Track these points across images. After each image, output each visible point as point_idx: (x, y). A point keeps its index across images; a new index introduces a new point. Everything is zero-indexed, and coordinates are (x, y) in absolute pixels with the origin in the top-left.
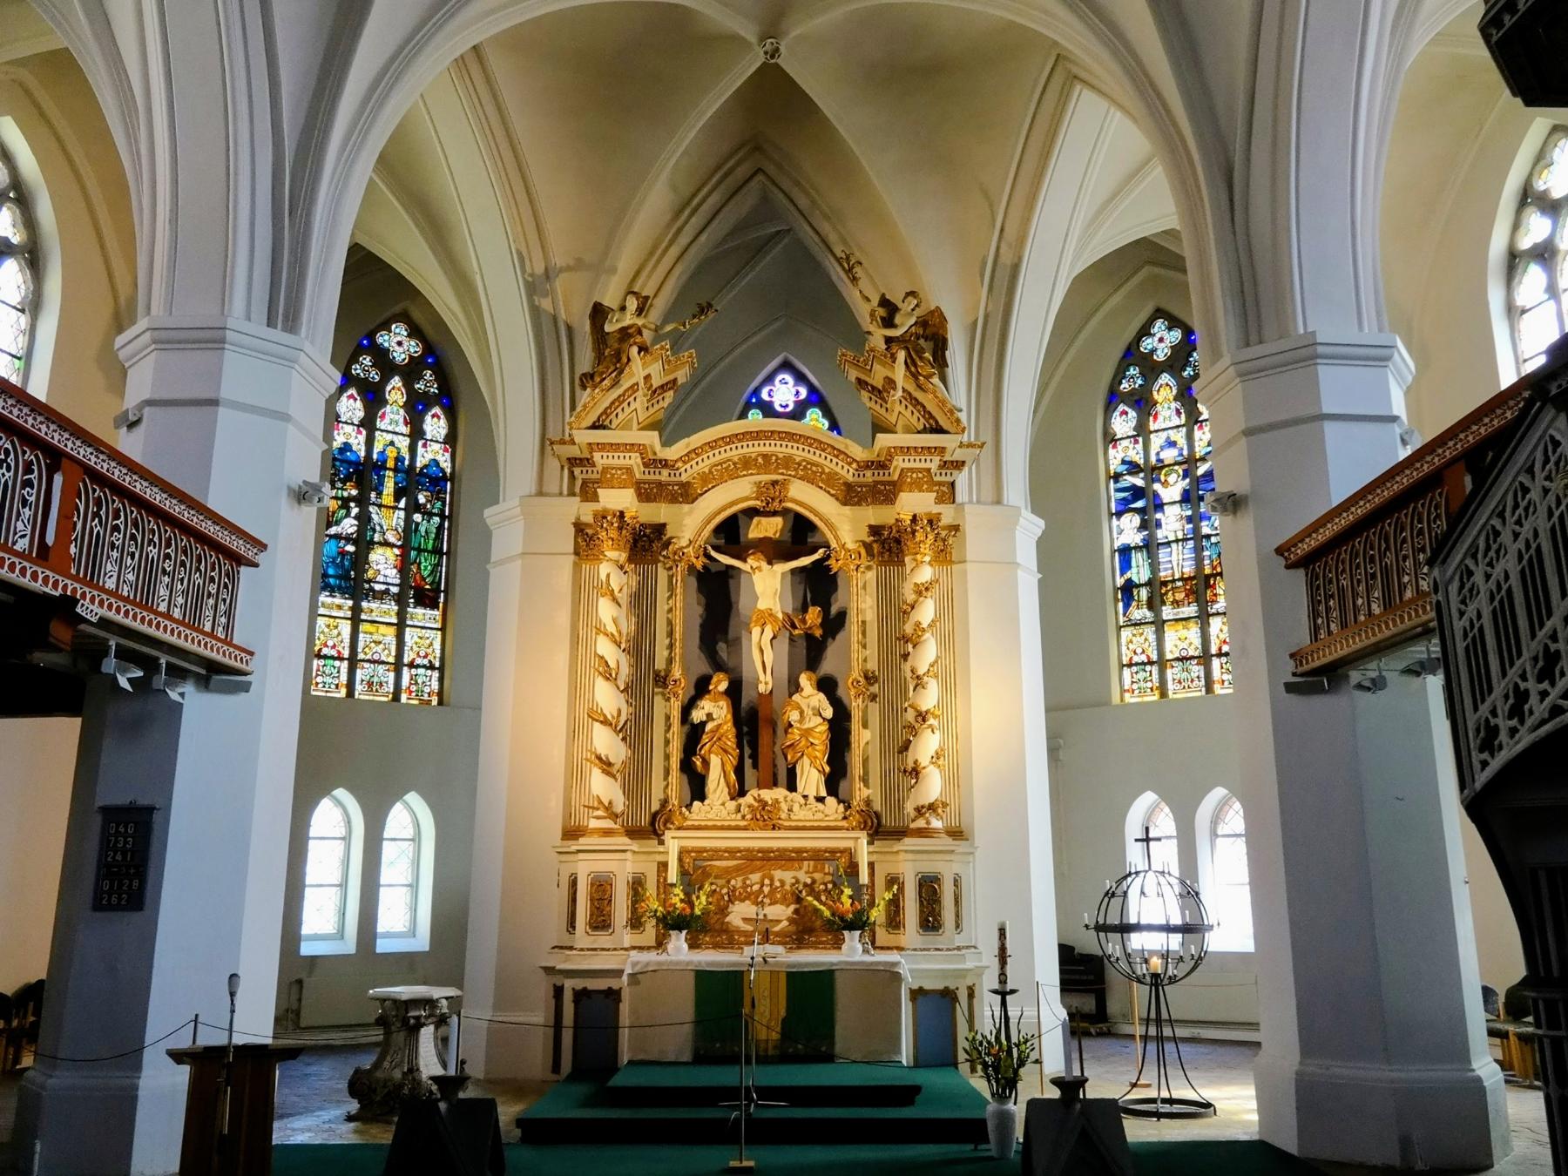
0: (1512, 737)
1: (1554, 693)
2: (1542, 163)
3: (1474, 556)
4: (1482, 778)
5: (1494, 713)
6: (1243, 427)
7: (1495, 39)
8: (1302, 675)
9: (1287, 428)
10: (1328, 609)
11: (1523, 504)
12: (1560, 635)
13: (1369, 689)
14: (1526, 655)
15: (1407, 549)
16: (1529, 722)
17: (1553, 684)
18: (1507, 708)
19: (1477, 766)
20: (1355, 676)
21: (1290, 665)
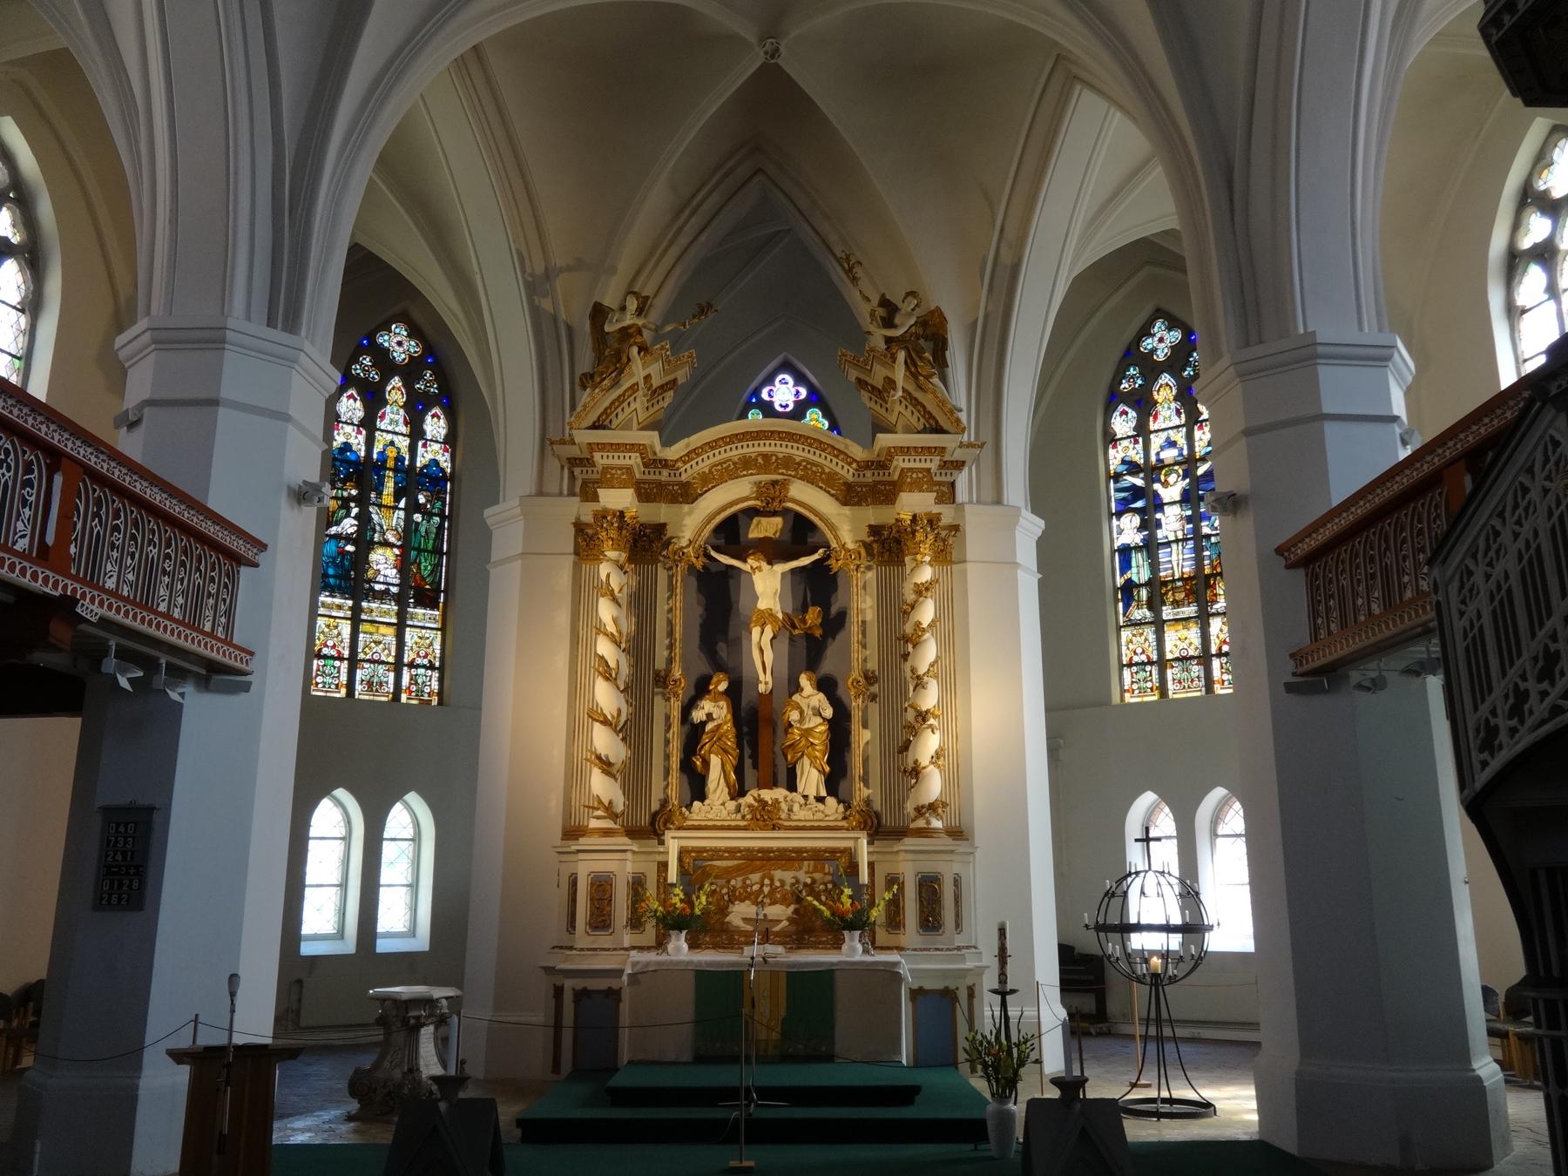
0: (1512, 737)
2: (1543, 163)
3: (1474, 556)
4: (1482, 778)
5: (1494, 713)
6: (1241, 426)
7: (1495, 38)
8: (1302, 675)
9: (1283, 426)
11: (1523, 504)
13: (1369, 689)
14: (1525, 655)
15: (1407, 549)
16: (1529, 722)
17: (1553, 684)
18: (1507, 707)
19: (1477, 766)
20: (1355, 676)
21: (1290, 666)
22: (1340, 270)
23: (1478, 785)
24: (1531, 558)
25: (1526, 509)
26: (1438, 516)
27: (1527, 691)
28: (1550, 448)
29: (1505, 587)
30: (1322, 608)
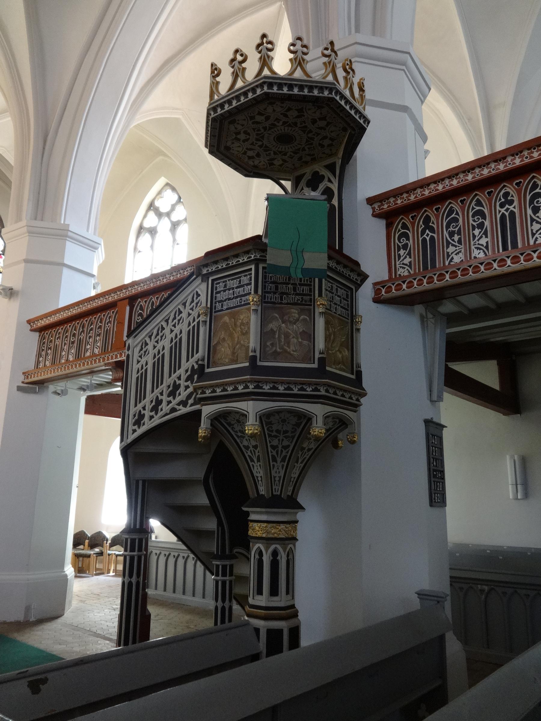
0: (150, 420)
1: (174, 402)
2: (160, 195)
3: (150, 337)
4: (132, 437)
5: (144, 408)
6: (24, 257)
7: (212, 116)
8: (27, 383)
9: (47, 265)
10: (47, 354)
11: (178, 318)
12: (182, 378)
13: (59, 394)
14: (165, 384)
15: (92, 333)
16: (160, 414)
17: (174, 398)
18: (151, 407)
19: (130, 431)
20: (52, 388)
21: (22, 378)
22: (82, 205)
23: (129, 440)
24: (176, 342)
25: (179, 320)
26: (110, 322)
27: (162, 400)
28: (195, 296)
29: (161, 353)
30: (43, 353)
